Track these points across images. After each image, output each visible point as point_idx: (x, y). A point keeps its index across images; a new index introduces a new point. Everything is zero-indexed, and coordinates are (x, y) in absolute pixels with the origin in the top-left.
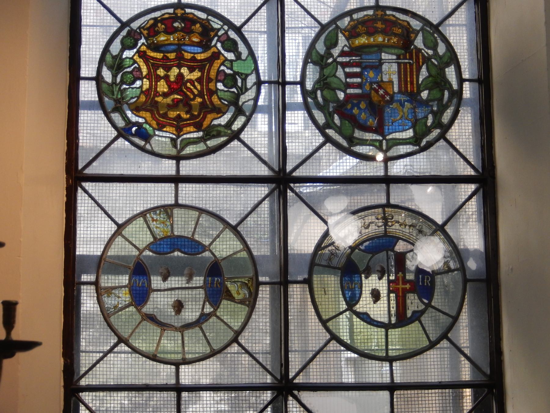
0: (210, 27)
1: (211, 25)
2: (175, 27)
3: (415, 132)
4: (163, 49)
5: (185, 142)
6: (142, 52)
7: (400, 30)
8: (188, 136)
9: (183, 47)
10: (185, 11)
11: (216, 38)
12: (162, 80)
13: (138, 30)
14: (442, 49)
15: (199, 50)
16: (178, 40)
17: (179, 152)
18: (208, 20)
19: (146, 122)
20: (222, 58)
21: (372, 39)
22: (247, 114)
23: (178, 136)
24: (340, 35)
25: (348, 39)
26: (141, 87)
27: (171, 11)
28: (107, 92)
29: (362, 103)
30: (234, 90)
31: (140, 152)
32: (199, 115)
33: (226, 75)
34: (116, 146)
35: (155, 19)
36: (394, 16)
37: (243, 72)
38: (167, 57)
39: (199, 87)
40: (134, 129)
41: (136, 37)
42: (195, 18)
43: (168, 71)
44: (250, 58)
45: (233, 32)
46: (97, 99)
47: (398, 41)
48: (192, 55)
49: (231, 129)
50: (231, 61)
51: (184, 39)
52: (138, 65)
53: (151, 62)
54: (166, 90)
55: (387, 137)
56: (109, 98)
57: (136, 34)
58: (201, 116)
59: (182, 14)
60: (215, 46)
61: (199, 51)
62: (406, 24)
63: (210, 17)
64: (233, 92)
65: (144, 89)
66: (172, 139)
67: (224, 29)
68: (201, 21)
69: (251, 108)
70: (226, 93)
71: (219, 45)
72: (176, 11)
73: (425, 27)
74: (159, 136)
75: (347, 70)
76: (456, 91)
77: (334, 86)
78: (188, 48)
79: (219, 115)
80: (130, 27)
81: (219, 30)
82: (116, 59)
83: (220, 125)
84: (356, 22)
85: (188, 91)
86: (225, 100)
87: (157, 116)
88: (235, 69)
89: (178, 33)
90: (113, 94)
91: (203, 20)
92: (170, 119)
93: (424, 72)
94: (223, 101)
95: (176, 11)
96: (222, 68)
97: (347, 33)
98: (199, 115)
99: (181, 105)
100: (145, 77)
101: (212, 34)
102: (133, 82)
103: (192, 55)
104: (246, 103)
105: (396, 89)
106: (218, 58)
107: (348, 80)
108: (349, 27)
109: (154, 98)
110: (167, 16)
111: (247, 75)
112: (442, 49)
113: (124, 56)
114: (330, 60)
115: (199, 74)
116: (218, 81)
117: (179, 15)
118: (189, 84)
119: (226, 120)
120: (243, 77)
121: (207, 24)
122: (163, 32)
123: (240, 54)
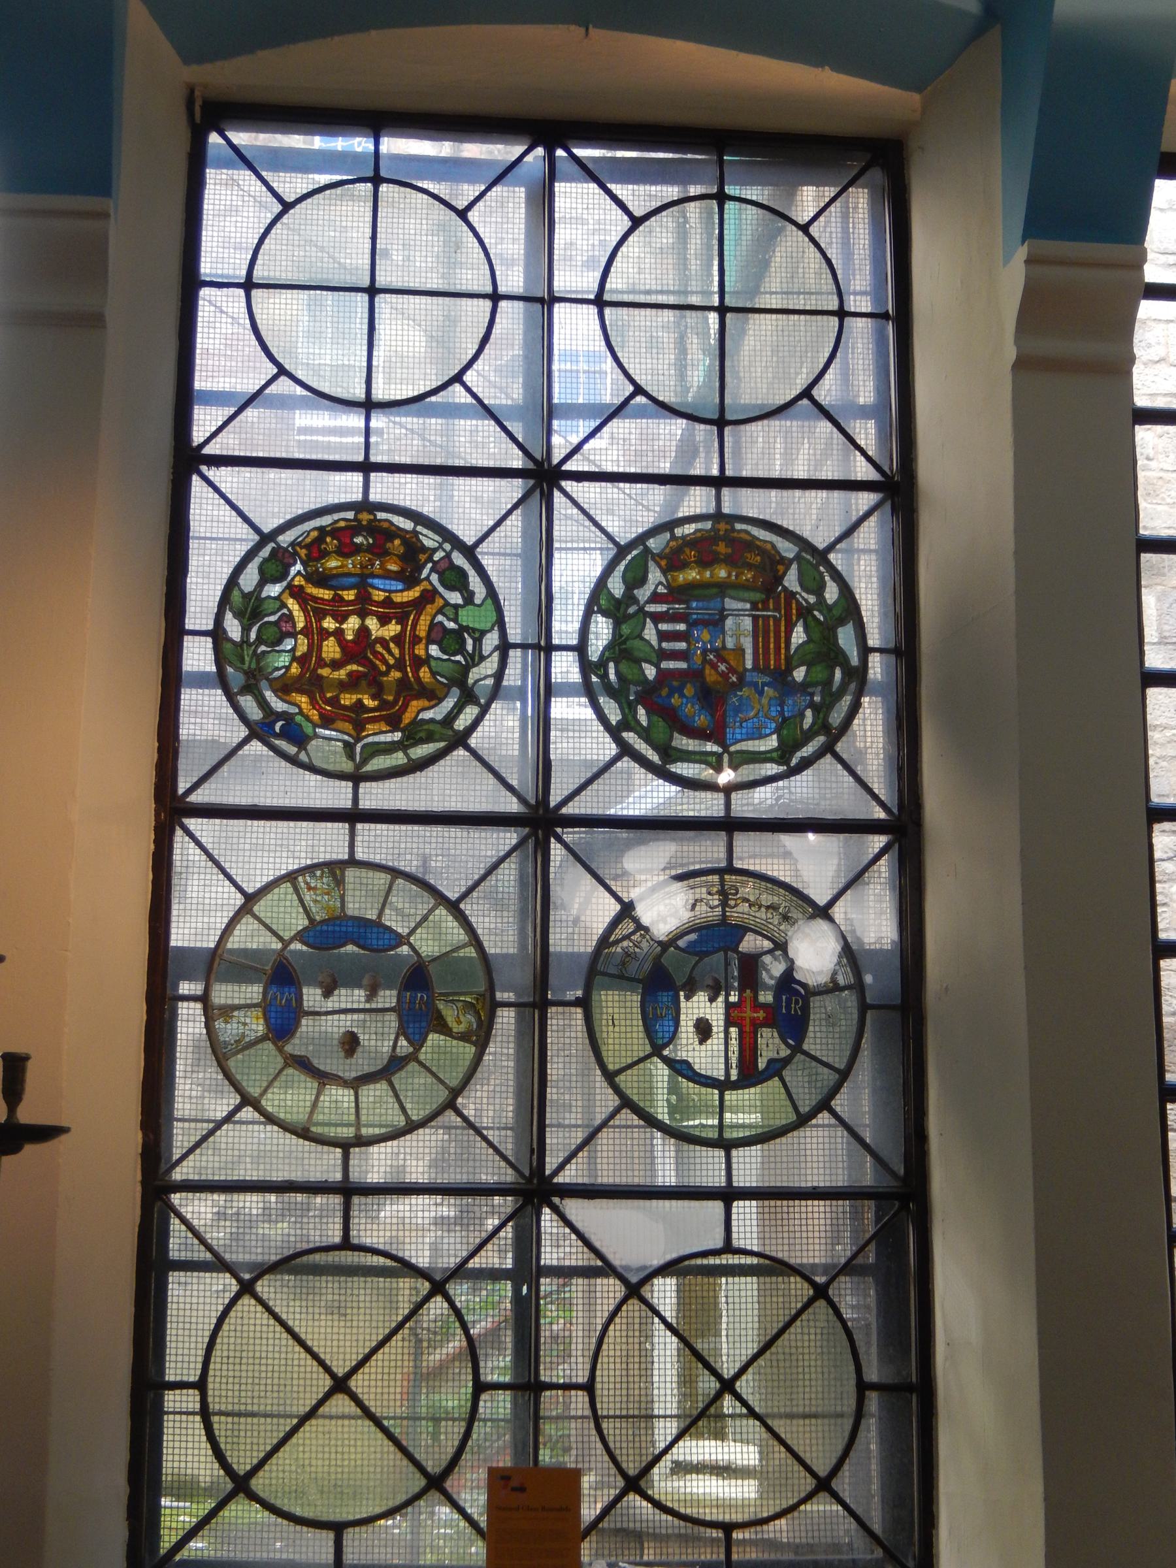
3: (779, 739)
4: (334, 583)
7: (758, 558)
8: (376, 739)
9: (370, 581)
11: (430, 565)
14: (831, 593)
16: (362, 567)
17: (358, 767)
18: (415, 533)
20: (440, 602)
21: (708, 574)
22: (482, 701)
23: (358, 739)
24: (652, 565)
25: (664, 572)
26: (293, 650)
27: (350, 515)
29: (689, 686)
30: (459, 658)
35: (321, 529)
36: (746, 532)
37: (477, 626)
41: (286, 561)
42: (393, 528)
44: (489, 601)
47: (754, 577)
49: (452, 728)
50: (456, 607)
51: (373, 565)
54: (338, 656)
55: (732, 749)
59: (370, 521)
60: (427, 578)
62: (769, 547)
63: (419, 528)
65: (298, 654)
66: (346, 744)
67: (444, 550)
69: (489, 691)
70: (445, 664)
71: (434, 578)
72: (360, 516)
73: (804, 554)
75: (664, 627)
76: (856, 669)
77: (637, 654)
80: (276, 543)
81: (435, 550)
83: (432, 721)
84: (680, 542)
90: (243, 662)
91: (406, 532)
92: (345, 708)
93: (799, 636)
95: (360, 516)
96: (440, 618)
97: (663, 563)
98: (396, 701)
99: (364, 683)
101: (423, 557)
102: (279, 642)
105: (749, 664)
107: (664, 645)
108: (667, 550)
109: (315, 670)
110: (342, 524)
111: (483, 633)
112: (831, 593)
114: (632, 610)
116: (430, 641)
118: (379, 648)
120: (477, 635)
122: (335, 552)
123: (472, 594)
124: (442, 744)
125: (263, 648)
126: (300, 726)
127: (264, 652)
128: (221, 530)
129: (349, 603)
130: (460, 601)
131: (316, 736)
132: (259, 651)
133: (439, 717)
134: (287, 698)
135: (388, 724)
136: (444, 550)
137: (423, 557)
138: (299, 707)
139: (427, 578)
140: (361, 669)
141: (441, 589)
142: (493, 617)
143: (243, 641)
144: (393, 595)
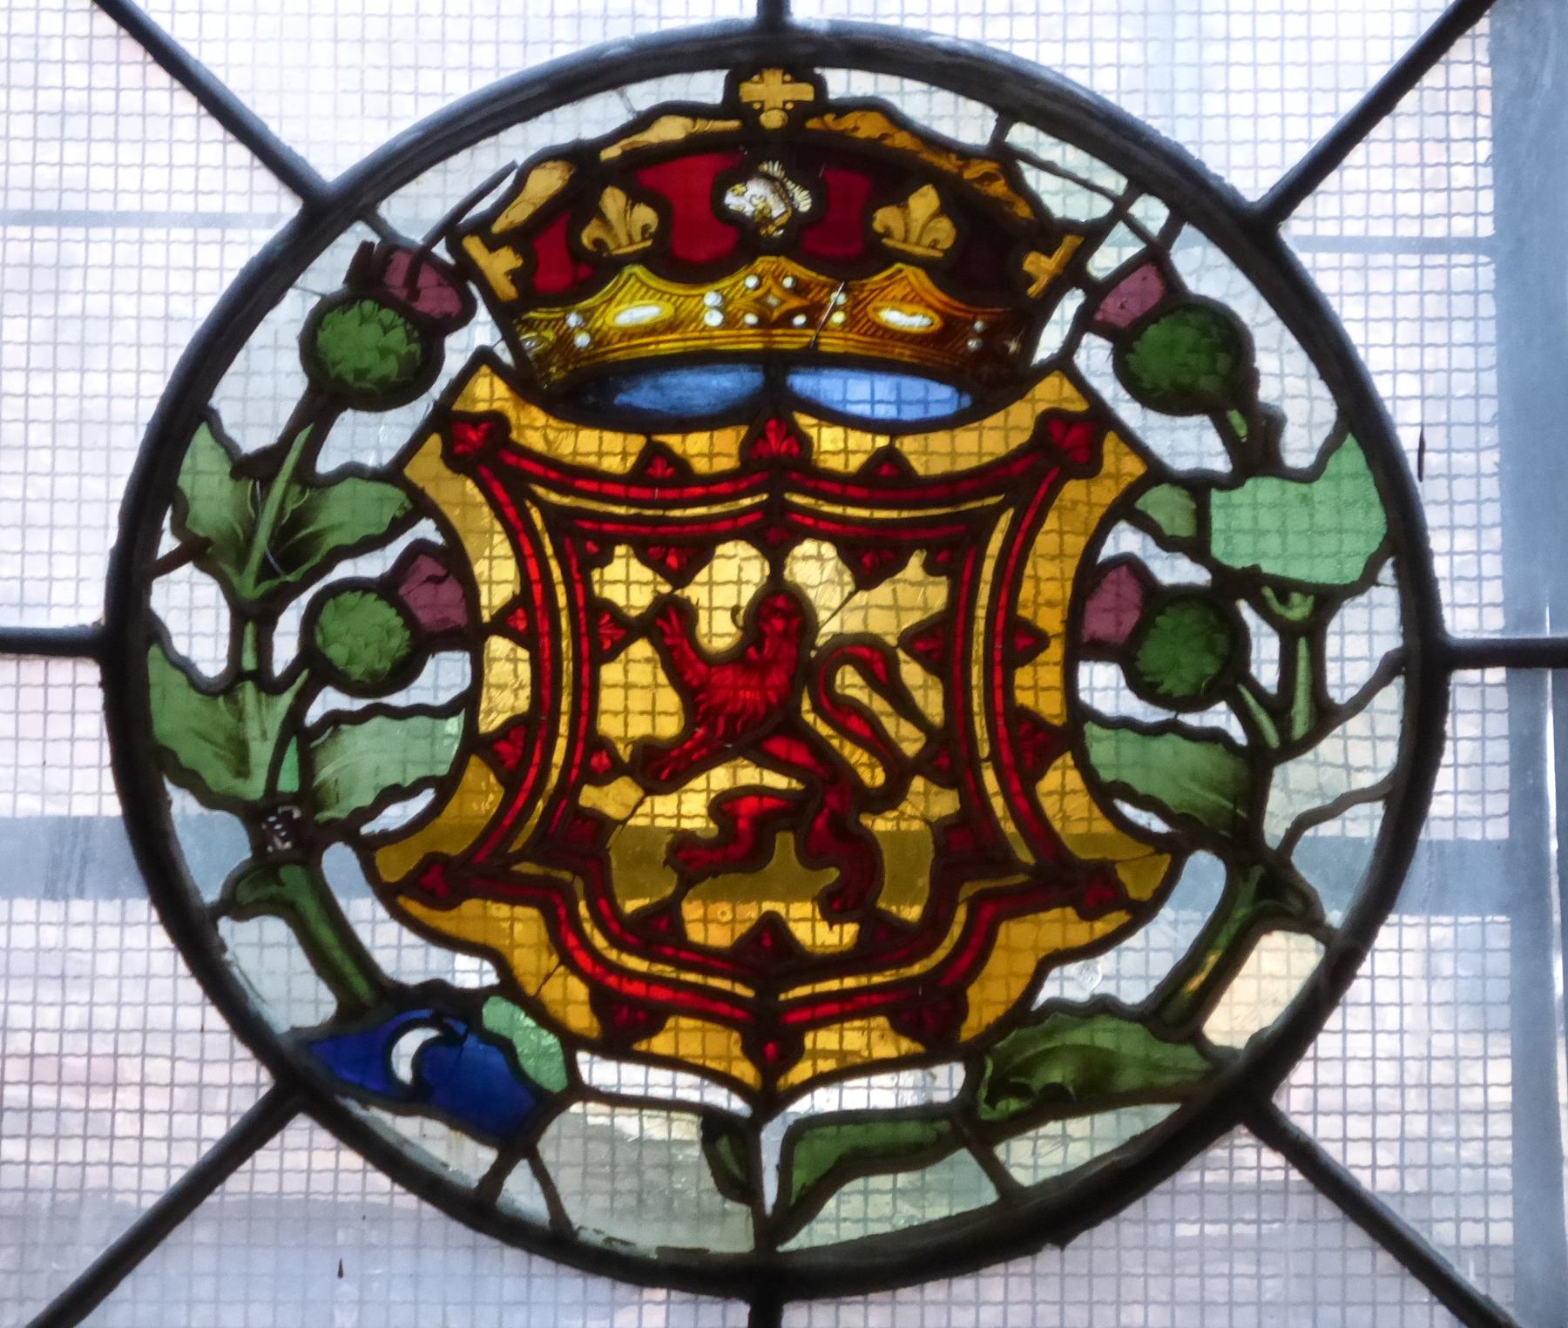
0: (1023, 211)
1: (1034, 201)
2: (736, 221)
4: (643, 396)
5: (824, 1150)
6: (476, 420)
8: (855, 1095)
9: (802, 383)
10: (820, 86)
11: (1071, 304)
12: (641, 649)
13: (440, 250)
15: (941, 398)
16: (764, 323)
17: (772, 1229)
18: (1004, 157)
19: (509, 988)
20: (1121, 466)
22: (1335, 917)
23: (768, 1101)
26: (468, 702)
27: (707, 87)
28: (190, 753)
30: (1220, 717)
31: (460, 1232)
32: (935, 922)
33: (1155, 597)
34: (266, 1185)
35: (579, 157)
37: (1298, 571)
38: (680, 465)
39: (932, 702)
40: (409, 1044)
41: (424, 305)
42: (901, 140)
43: (681, 578)
44: (1351, 457)
45: (1216, 256)
46: (113, 807)
48: (882, 441)
49: (1196, 1039)
50: (1199, 486)
51: (814, 312)
52: (444, 526)
53: (544, 506)
54: (670, 727)
56: (210, 799)
57: (427, 278)
58: (956, 931)
59: (798, 113)
60: (1063, 362)
61: (937, 411)
63: (1022, 135)
64: (1216, 737)
65: (490, 722)
66: (713, 1123)
67: (1138, 230)
68: (948, 164)
69: (1363, 863)
70: (1167, 746)
71: (1095, 357)
72: (751, 91)
74: (616, 1100)
78: (830, 387)
79: (1102, 927)
80: (377, 225)
81: (1094, 234)
82: (267, 482)
83: (1103, 1007)
85: (844, 731)
86: (1146, 802)
87: (600, 941)
88: (1232, 548)
89: (763, 263)
90: (242, 768)
91: (966, 154)
92: (707, 959)
94: (1128, 810)
95: (751, 91)
96: (1125, 540)
98: (935, 922)
99: (785, 844)
100: (503, 623)
101: (1041, 267)
102: (405, 671)
103: (882, 441)
104: (1328, 829)
106: (1090, 467)
109: (569, 788)
110: (672, 130)
111: (1328, 600)
113: (326, 463)
115: (937, 595)
116: (1081, 648)
117: (772, 120)
118: (850, 682)
119: (1162, 966)
120: (1299, 609)
121: (999, 188)
122: (641, 258)
123: (1268, 426)
124: (1161, 1112)
125: (329, 700)
126: (505, 1046)
127: (335, 719)
128: (129, 179)
129: (715, 487)
130: (1220, 463)
131: (579, 1090)
132: (314, 714)
133: (1134, 993)
134: (444, 921)
135: (900, 1027)
136: (1138, 230)
137: (1041, 267)
138: (501, 963)
139: (1063, 362)
140: (169, 513)
141: (1129, 412)
142: (1372, 523)
143: (235, 675)
144: (908, 445)
